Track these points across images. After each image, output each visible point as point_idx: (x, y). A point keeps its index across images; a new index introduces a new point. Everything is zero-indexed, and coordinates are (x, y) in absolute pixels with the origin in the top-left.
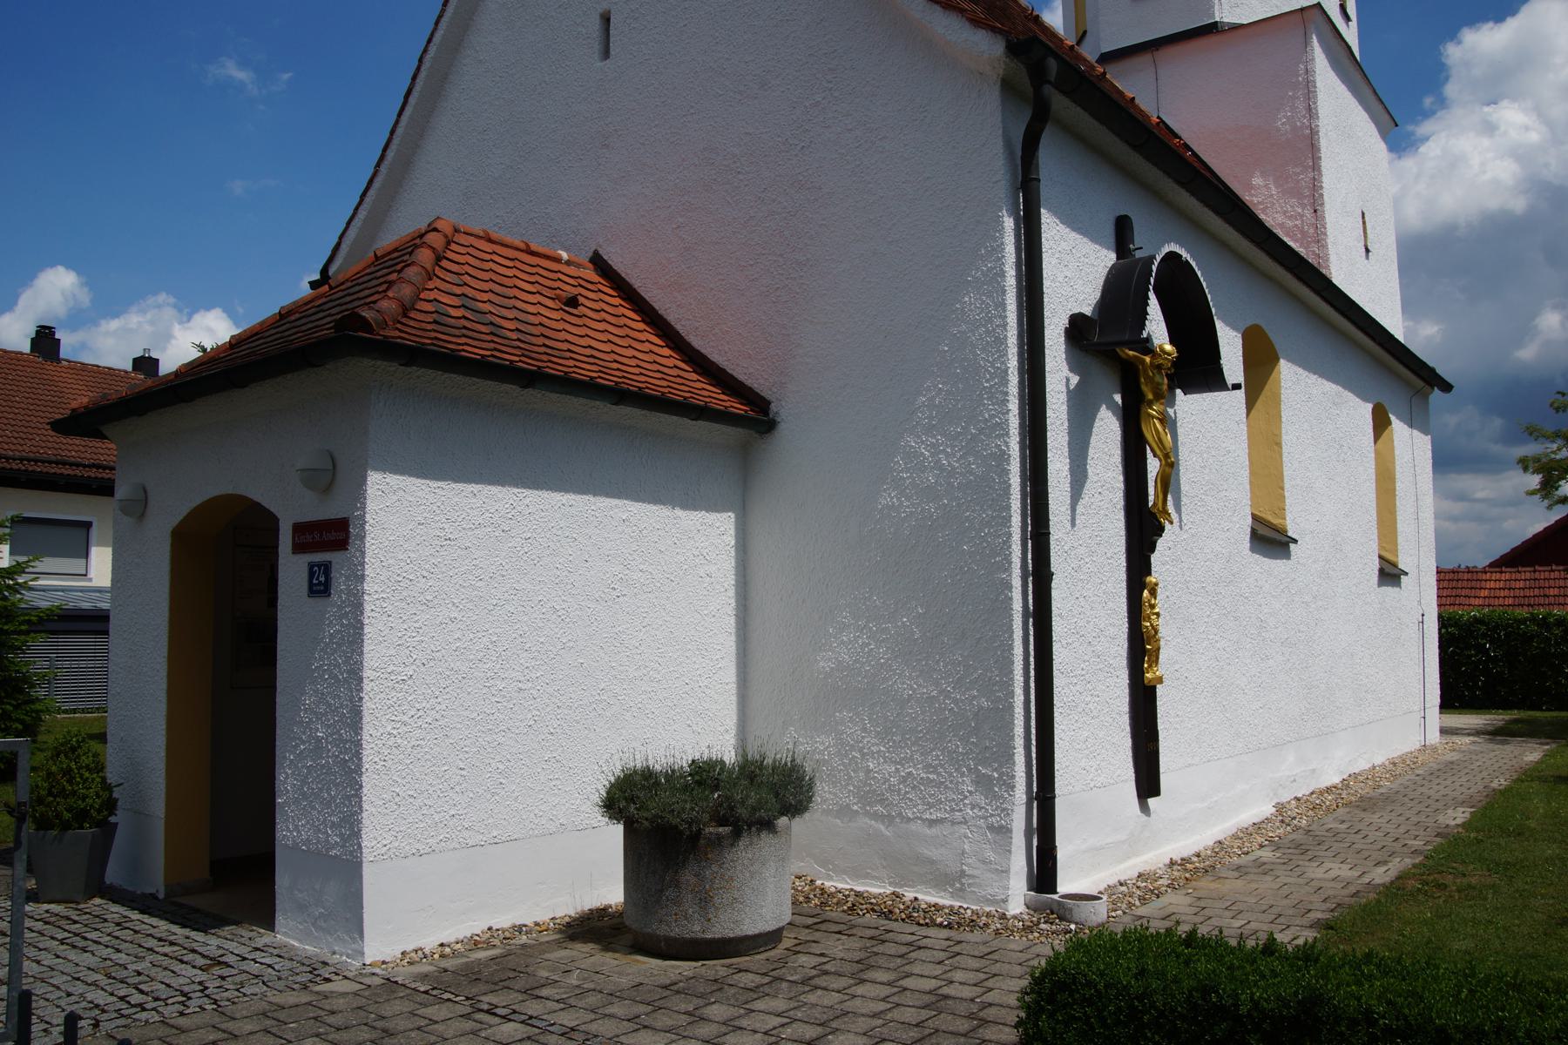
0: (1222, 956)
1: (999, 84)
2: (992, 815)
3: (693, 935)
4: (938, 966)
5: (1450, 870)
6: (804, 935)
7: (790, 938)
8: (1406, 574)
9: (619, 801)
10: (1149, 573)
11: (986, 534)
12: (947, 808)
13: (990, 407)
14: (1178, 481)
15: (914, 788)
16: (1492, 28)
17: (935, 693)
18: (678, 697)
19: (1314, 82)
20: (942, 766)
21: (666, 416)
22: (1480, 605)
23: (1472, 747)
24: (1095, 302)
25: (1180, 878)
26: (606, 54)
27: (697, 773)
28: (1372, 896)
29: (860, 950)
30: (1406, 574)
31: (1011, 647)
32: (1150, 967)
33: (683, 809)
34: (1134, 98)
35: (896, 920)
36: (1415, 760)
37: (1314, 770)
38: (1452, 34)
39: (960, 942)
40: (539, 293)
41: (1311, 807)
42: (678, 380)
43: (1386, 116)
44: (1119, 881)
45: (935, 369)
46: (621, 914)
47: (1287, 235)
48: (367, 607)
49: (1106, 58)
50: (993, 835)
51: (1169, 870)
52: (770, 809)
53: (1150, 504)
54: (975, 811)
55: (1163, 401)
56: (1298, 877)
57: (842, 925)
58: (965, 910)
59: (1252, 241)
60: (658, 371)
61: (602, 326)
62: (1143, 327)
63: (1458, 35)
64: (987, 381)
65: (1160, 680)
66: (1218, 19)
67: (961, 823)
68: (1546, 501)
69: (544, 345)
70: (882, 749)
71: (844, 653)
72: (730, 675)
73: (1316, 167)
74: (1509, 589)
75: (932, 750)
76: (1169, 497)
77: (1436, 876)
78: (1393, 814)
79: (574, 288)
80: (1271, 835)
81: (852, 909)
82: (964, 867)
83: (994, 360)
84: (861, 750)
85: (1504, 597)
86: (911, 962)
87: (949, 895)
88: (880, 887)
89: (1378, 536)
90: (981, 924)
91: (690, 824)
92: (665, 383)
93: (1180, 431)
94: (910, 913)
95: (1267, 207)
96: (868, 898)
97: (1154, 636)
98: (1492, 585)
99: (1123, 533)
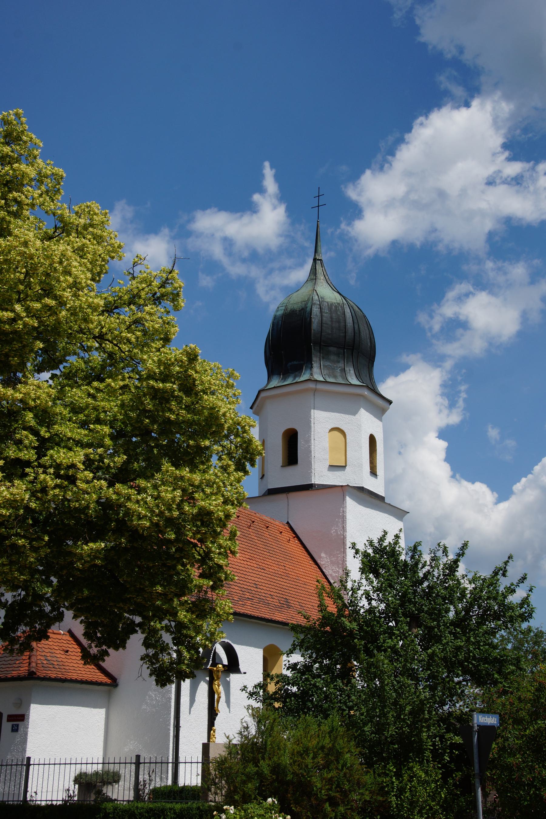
10: (214, 726)
48: (29, 734)
66: (313, 483)
99: (207, 715)
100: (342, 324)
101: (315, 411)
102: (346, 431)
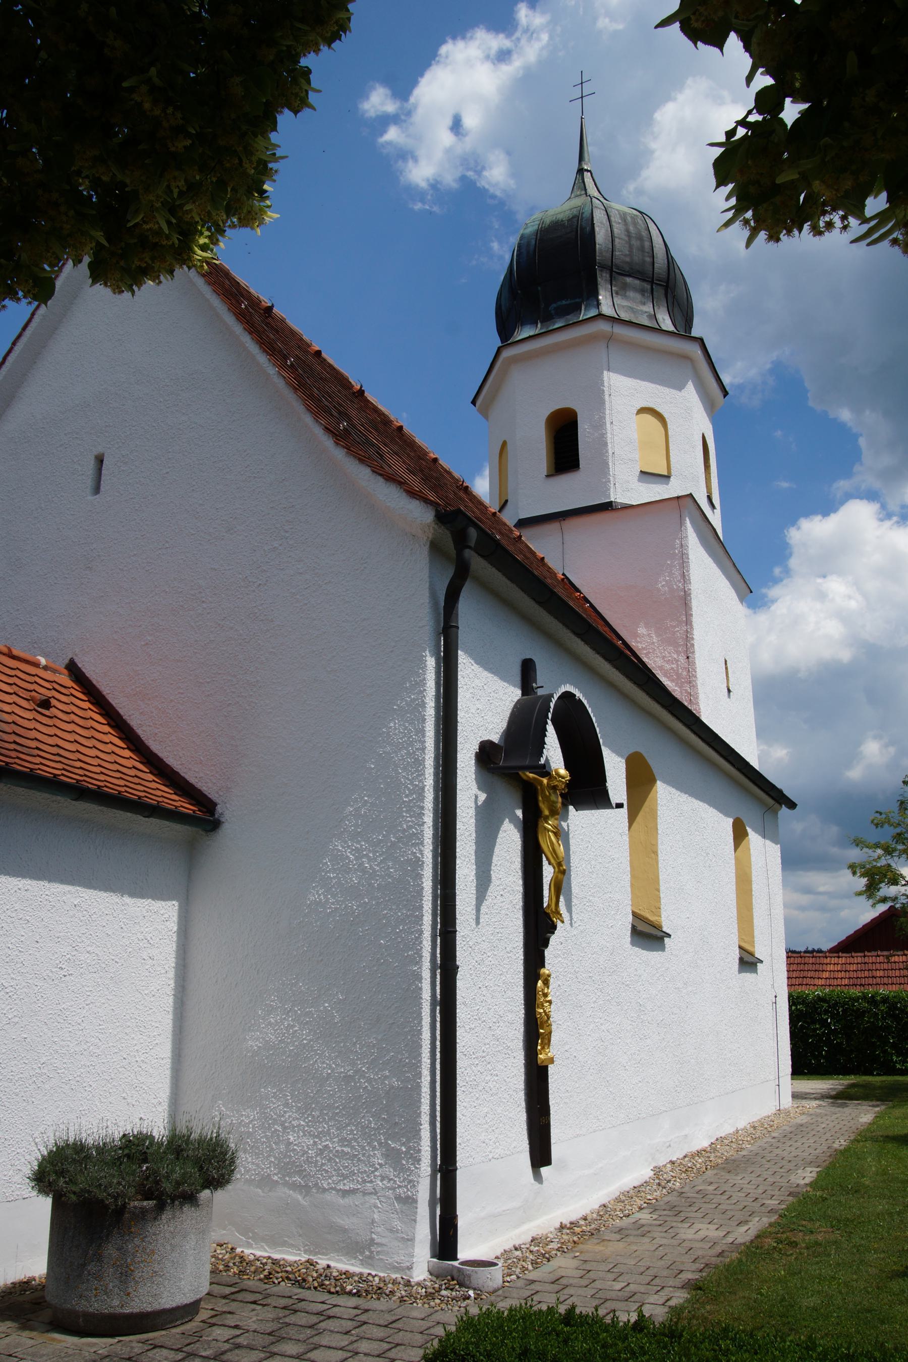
0: (597, 1333)
1: (427, 546)
2: (399, 1187)
3: (112, 1310)
4: (345, 1336)
5: (800, 1228)
6: (221, 1305)
7: (207, 1309)
8: (761, 962)
9: (49, 1174)
10: (543, 966)
11: (401, 931)
12: (359, 1179)
13: (408, 819)
14: (569, 884)
15: (330, 1160)
16: (821, 521)
17: (351, 1073)
18: (116, 1071)
19: (687, 554)
20: (356, 1140)
21: (122, 812)
22: (822, 985)
23: (818, 1111)
24: (502, 731)
25: (569, 1241)
26: (97, 489)
27: (127, 1146)
28: (735, 1255)
29: (273, 1321)
30: (761, 962)
31: (420, 1032)
32: (532, 1347)
33: (110, 1185)
34: (543, 558)
35: (309, 1288)
36: (772, 1123)
37: (686, 1135)
38: (793, 521)
39: (366, 1311)
40: (15, 693)
41: (684, 1170)
42: (136, 780)
43: (744, 584)
44: (514, 1246)
45: (362, 783)
46: (43, 1287)
47: (665, 676)
49: (523, 523)
50: (400, 1205)
51: (559, 1234)
52: (193, 1184)
53: (545, 905)
54: (385, 1182)
55: (557, 817)
56: (672, 1238)
57: (258, 1294)
58: (374, 1277)
59: (635, 683)
60: (118, 771)
61: (70, 727)
62: (541, 754)
63: (798, 522)
64: (407, 796)
65: (552, 1060)
66: (613, 500)
67: (371, 1193)
68: (871, 901)
69: (15, 742)
70: (302, 1123)
71: (271, 1034)
72: (165, 1050)
73: (688, 622)
74: (845, 971)
75: (348, 1125)
76: (562, 899)
77: (788, 1234)
78: (753, 1175)
79: (48, 691)
80: (649, 1197)
81: (267, 1277)
82: (374, 1236)
83: (413, 778)
84: (282, 1125)
85: (841, 978)
86: (320, 1333)
87: (359, 1262)
88: (296, 1255)
89: (739, 930)
90: (387, 1292)
91: (116, 1199)
92: (122, 783)
93: (572, 841)
94: (322, 1281)
95: (649, 653)
96: (285, 1266)
97: (547, 1021)
98: (832, 967)
99: (521, 929)
100: (647, 244)
101: (611, 374)
102: (666, 415)
